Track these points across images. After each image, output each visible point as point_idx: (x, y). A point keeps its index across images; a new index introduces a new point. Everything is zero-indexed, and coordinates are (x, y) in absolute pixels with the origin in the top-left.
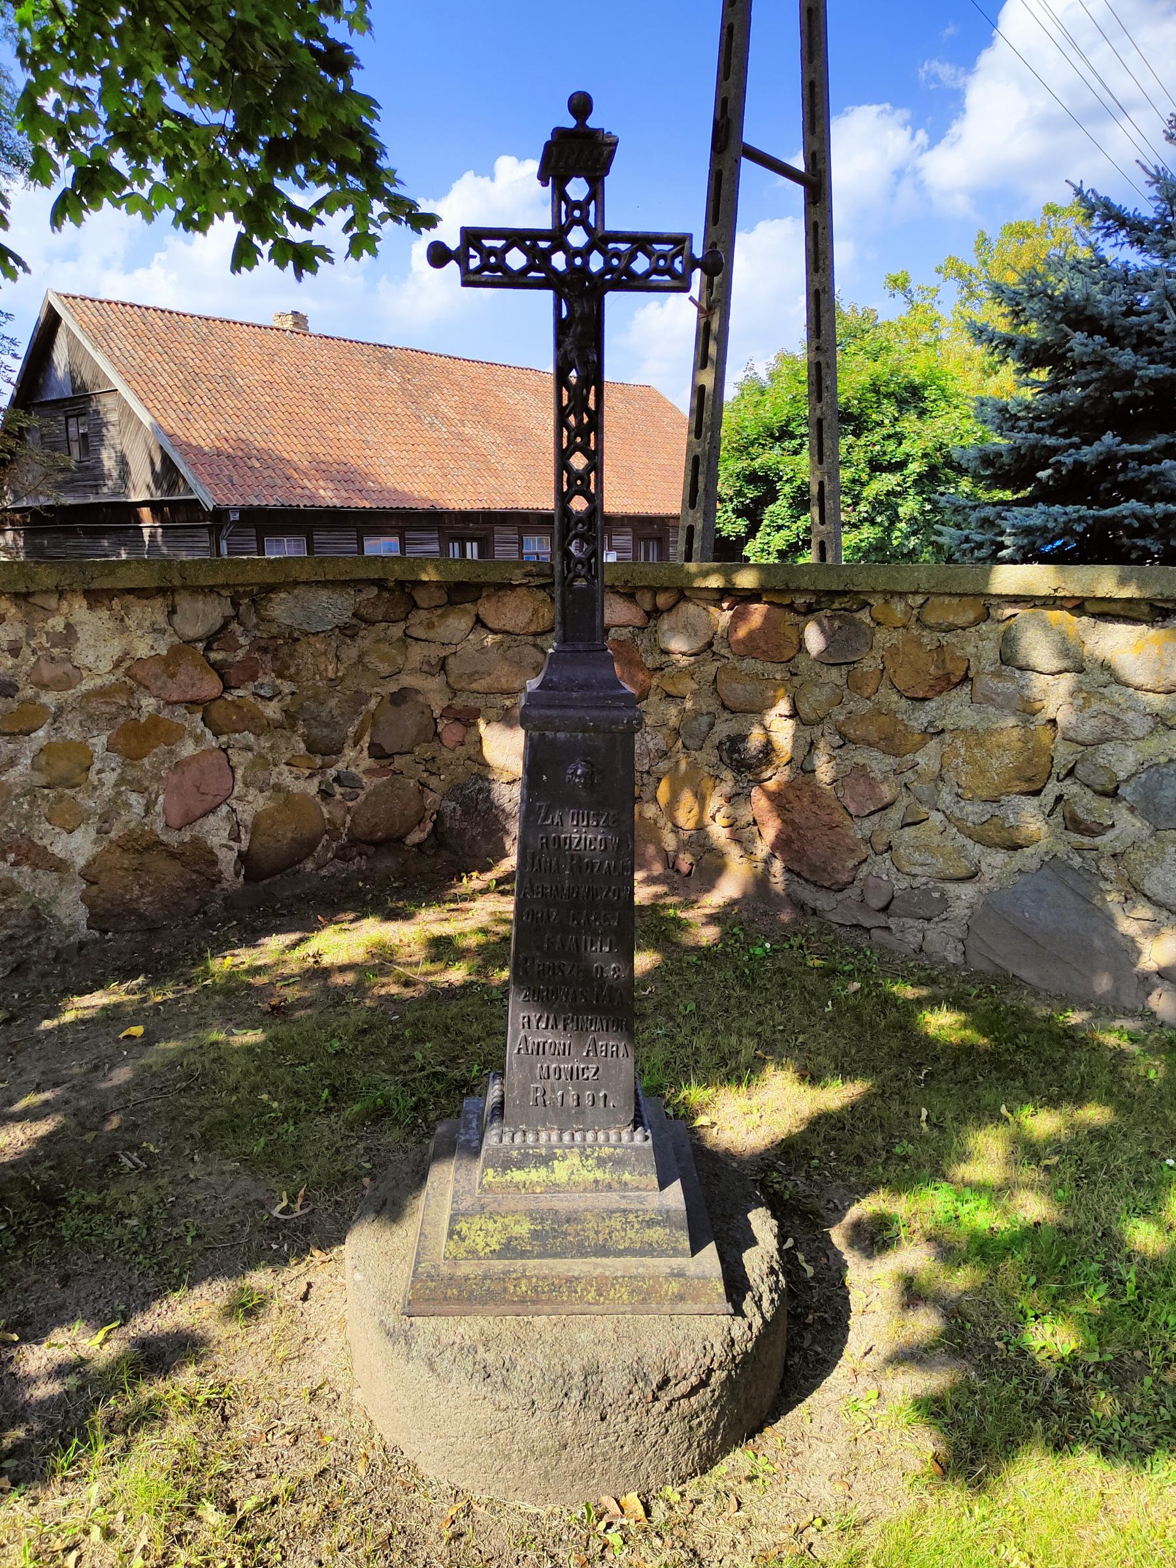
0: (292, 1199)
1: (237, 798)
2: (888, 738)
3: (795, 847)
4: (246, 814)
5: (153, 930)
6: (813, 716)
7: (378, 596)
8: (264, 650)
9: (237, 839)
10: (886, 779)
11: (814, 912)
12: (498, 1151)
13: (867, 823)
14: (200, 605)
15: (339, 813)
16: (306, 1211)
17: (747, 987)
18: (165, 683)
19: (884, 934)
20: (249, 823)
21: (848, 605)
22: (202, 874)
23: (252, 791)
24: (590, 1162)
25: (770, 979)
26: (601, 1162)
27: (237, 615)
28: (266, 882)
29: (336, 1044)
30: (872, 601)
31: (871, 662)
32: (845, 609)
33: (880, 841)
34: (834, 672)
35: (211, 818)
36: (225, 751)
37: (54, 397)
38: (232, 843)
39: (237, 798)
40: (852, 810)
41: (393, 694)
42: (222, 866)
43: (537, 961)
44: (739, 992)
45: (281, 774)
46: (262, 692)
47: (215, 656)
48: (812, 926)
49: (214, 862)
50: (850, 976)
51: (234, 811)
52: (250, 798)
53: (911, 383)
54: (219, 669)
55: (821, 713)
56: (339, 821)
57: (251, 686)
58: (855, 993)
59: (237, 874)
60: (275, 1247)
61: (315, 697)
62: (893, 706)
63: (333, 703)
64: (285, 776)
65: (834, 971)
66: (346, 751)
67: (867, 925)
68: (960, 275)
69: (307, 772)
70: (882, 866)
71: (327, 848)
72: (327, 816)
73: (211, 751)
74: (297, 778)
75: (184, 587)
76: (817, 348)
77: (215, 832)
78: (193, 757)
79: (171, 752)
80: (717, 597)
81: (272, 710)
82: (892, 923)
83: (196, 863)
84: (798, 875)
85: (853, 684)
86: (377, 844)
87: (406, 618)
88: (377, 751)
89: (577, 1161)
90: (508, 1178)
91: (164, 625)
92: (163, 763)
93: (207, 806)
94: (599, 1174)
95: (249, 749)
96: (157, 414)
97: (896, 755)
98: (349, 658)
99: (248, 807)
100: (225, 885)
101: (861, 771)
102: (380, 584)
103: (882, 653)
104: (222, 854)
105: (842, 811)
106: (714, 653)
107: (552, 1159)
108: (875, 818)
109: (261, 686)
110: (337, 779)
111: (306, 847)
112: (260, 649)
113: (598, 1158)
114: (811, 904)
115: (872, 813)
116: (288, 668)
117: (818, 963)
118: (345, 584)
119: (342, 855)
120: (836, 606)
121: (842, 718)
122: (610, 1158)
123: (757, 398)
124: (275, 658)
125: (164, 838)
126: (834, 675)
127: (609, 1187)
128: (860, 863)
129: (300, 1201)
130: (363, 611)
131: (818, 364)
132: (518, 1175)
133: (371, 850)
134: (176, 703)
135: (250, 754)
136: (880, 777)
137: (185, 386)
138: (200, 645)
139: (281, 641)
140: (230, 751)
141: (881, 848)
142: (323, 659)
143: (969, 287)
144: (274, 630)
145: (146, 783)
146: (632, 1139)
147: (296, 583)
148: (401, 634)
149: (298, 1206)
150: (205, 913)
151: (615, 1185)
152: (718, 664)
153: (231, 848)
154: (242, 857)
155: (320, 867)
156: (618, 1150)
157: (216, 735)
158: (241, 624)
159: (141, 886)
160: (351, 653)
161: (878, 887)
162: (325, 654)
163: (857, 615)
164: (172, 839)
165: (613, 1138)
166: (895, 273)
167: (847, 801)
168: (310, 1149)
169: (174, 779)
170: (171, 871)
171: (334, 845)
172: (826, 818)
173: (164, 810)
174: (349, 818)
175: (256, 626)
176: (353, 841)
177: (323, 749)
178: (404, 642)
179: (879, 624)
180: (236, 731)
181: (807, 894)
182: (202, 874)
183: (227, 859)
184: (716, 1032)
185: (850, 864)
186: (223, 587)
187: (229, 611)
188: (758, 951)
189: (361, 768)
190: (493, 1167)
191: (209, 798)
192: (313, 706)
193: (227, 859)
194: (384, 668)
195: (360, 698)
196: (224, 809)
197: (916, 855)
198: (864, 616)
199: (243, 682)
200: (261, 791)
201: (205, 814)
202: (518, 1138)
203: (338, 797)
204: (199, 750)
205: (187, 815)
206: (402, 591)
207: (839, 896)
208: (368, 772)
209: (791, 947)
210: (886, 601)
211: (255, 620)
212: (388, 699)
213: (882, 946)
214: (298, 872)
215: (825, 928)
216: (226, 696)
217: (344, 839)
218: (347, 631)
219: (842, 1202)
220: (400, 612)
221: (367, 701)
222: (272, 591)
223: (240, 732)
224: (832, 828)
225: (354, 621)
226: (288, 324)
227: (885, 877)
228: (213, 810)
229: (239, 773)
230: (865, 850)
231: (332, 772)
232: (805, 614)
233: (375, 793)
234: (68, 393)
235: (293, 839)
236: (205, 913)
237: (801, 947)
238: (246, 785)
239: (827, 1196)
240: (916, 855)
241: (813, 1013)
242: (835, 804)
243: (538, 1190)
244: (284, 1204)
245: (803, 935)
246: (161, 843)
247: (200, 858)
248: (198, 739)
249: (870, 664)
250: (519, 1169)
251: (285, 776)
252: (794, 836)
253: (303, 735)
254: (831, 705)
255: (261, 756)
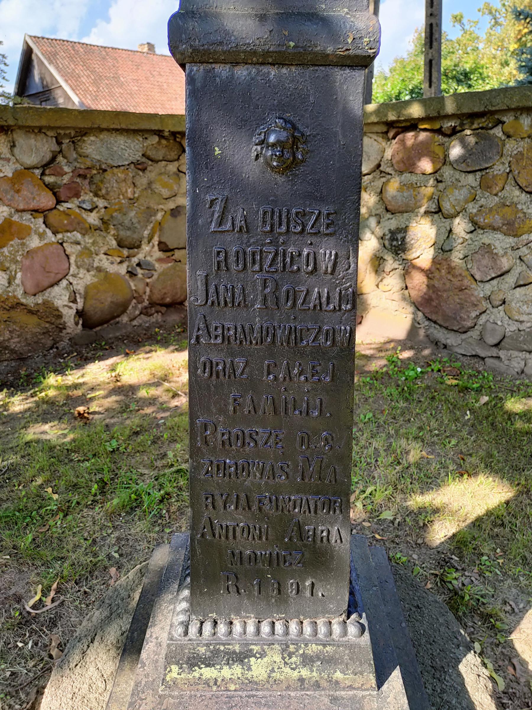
0: (45, 594)
1: (72, 275)
2: (510, 224)
3: (434, 304)
4: (79, 285)
5: (22, 359)
6: (452, 211)
7: (159, 143)
8: (83, 177)
9: (74, 301)
10: (506, 253)
11: (445, 347)
12: (182, 647)
13: (488, 286)
14: (32, 141)
15: (141, 286)
16: (56, 604)
17: (407, 400)
18: (13, 196)
19: (496, 362)
20: (82, 291)
21: (484, 125)
22: (53, 324)
23: (82, 270)
24: (294, 659)
25: (422, 395)
26: (308, 661)
27: (61, 151)
28: (98, 328)
29: (114, 444)
30: (505, 119)
31: (501, 167)
32: (482, 128)
33: (497, 299)
34: (471, 177)
35: (56, 288)
36: (61, 244)
37: (34, 92)
38: (71, 304)
39: (72, 275)
40: (477, 277)
41: (172, 210)
42: (65, 319)
43: (220, 429)
44: (402, 404)
45: (101, 260)
46: (84, 206)
47: (50, 179)
48: (444, 355)
49: (60, 316)
50: (479, 391)
51: (71, 284)
52: (81, 275)
53: (465, 70)
54: (52, 188)
55: (458, 209)
56: (141, 292)
57: (76, 201)
58: (486, 404)
59: (77, 324)
60: (20, 645)
61: (120, 210)
62: (515, 199)
63: (132, 214)
64: (104, 262)
65: (467, 388)
66: (143, 246)
67: (483, 355)
68: (490, 13)
69: (118, 259)
70: (498, 315)
71: (135, 308)
72: (134, 288)
73: (51, 244)
74: (112, 263)
75: (21, 127)
76: (431, 15)
77: (59, 297)
78: (39, 248)
79: (23, 244)
80: (385, 129)
81: (93, 219)
82: (502, 354)
83: (47, 317)
84: (435, 322)
85: (485, 185)
86: (168, 306)
87: (178, 159)
88: (164, 247)
89: (278, 658)
90: (196, 674)
91: (8, 156)
92: (18, 251)
93: (52, 280)
94: (305, 673)
95: (78, 243)
96: (81, 97)
97: (515, 236)
98: (142, 185)
99: (79, 281)
100: (69, 330)
101: (487, 249)
102: (159, 133)
103: (509, 159)
104: (65, 311)
105: (469, 278)
106: (381, 172)
107: (248, 657)
108: (495, 282)
109: (84, 202)
110: (139, 265)
111: (123, 308)
112: (80, 176)
113: (304, 655)
114: (443, 341)
115: (493, 279)
116: (100, 190)
117: (455, 382)
118: (136, 132)
119: (145, 312)
120: (475, 126)
121: (475, 211)
122: (317, 657)
123: (383, 82)
124: (91, 183)
125: (23, 301)
126: (471, 180)
127: (317, 685)
128: (481, 314)
129: (52, 594)
130: (149, 153)
131: (431, 25)
132: (208, 673)
133: (164, 309)
134: (23, 211)
135: (79, 247)
136: (501, 252)
137: (95, 83)
138: (38, 172)
139: (95, 172)
140: (65, 245)
141: (498, 303)
142: (124, 184)
143: (495, 19)
144: (89, 163)
145: (7, 265)
146: (345, 633)
147: (101, 130)
148: (175, 170)
149: (49, 599)
150: (57, 348)
151: (324, 684)
152: (384, 180)
153: (70, 308)
154: (80, 314)
155: (132, 320)
156: (328, 648)
157: (55, 233)
158: (64, 157)
159: (10, 332)
160: (143, 180)
161: (494, 330)
162: (125, 180)
163: (492, 132)
164: (30, 301)
165: (322, 630)
166: (456, 13)
167: (475, 271)
168: (71, 541)
169: (27, 262)
170: (32, 324)
171: (140, 306)
172: (458, 284)
173: (22, 283)
174: (148, 290)
175: (76, 160)
176: (152, 304)
177: (128, 245)
178: (178, 175)
179: (509, 137)
180: (67, 231)
181: (441, 335)
182: (53, 324)
183: (69, 315)
184: (389, 436)
185: (473, 314)
186: (50, 128)
187: (56, 148)
188: (412, 373)
189: (154, 258)
190: (177, 663)
191: (52, 275)
192: (119, 216)
193: (69, 315)
194: (165, 193)
195: (150, 212)
196: (64, 283)
197: (525, 307)
198: (498, 132)
199: (70, 198)
200: (88, 271)
201: (52, 286)
202: (208, 627)
203: (140, 276)
204: (43, 243)
205: (37, 285)
206: (175, 140)
207: (464, 336)
208: (159, 260)
209: (433, 370)
210: (516, 118)
211: (75, 156)
212: (169, 213)
213: (494, 370)
214: (118, 323)
215: (453, 357)
216: (58, 207)
217: (146, 303)
218: (140, 166)
219: (517, 604)
220: (173, 155)
221: (155, 214)
222: (85, 134)
223: (71, 232)
224: (461, 290)
225: (144, 160)
226: (146, 49)
227: (499, 323)
228: (57, 283)
229: (72, 259)
230: (485, 304)
231: (135, 260)
232: (450, 136)
233: (163, 274)
234: (41, 90)
235: (112, 302)
236: (57, 348)
237: (439, 371)
238: (78, 267)
239: (502, 596)
240: (525, 307)
241: (457, 420)
242: (465, 273)
243: (232, 687)
244: (37, 598)
245: (440, 362)
246: (22, 304)
247: (52, 313)
248: (41, 236)
249: (499, 168)
250: (207, 666)
251: (104, 262)
252: (434, 296)
253: (114, 235)
254: (467, 202)
255: (86, 248)
